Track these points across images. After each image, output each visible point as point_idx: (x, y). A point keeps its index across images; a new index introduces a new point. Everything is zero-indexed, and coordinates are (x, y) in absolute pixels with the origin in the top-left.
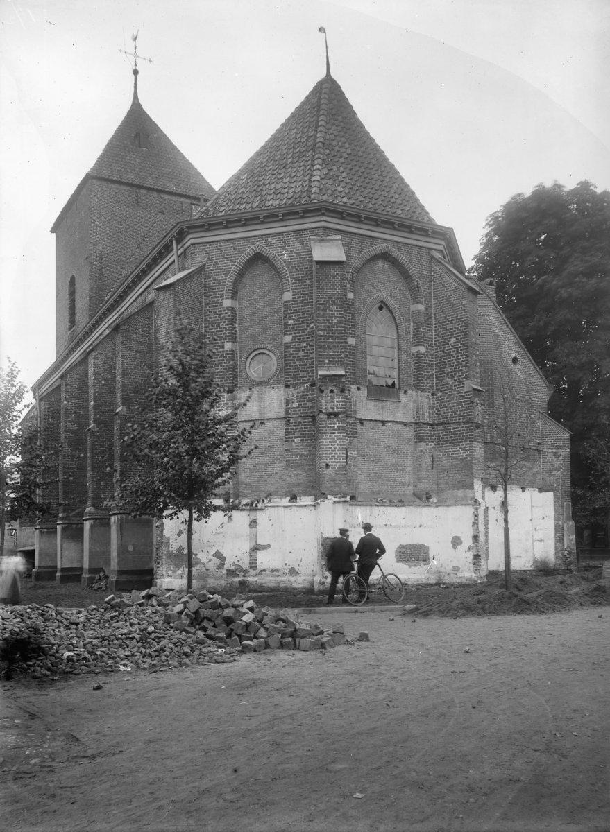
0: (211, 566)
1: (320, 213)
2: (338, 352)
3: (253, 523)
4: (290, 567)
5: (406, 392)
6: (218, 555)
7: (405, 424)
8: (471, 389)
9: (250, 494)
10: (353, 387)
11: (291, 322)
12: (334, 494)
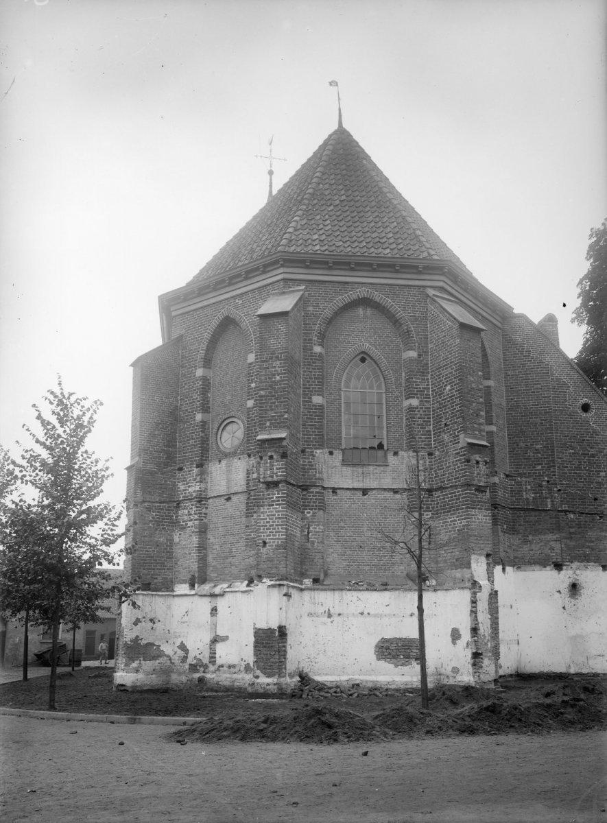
0: (176, 659)
1: (279, 265)
2: (281, 412)
3: (214, 611)
4: (246, 663)
5: (396, 454)
6: (183, 647)
7: (395, 491)
8: (466, 445)
9: (217, 577)
10: (318, 451)
11: (253, 385)
12: (270, 576)
